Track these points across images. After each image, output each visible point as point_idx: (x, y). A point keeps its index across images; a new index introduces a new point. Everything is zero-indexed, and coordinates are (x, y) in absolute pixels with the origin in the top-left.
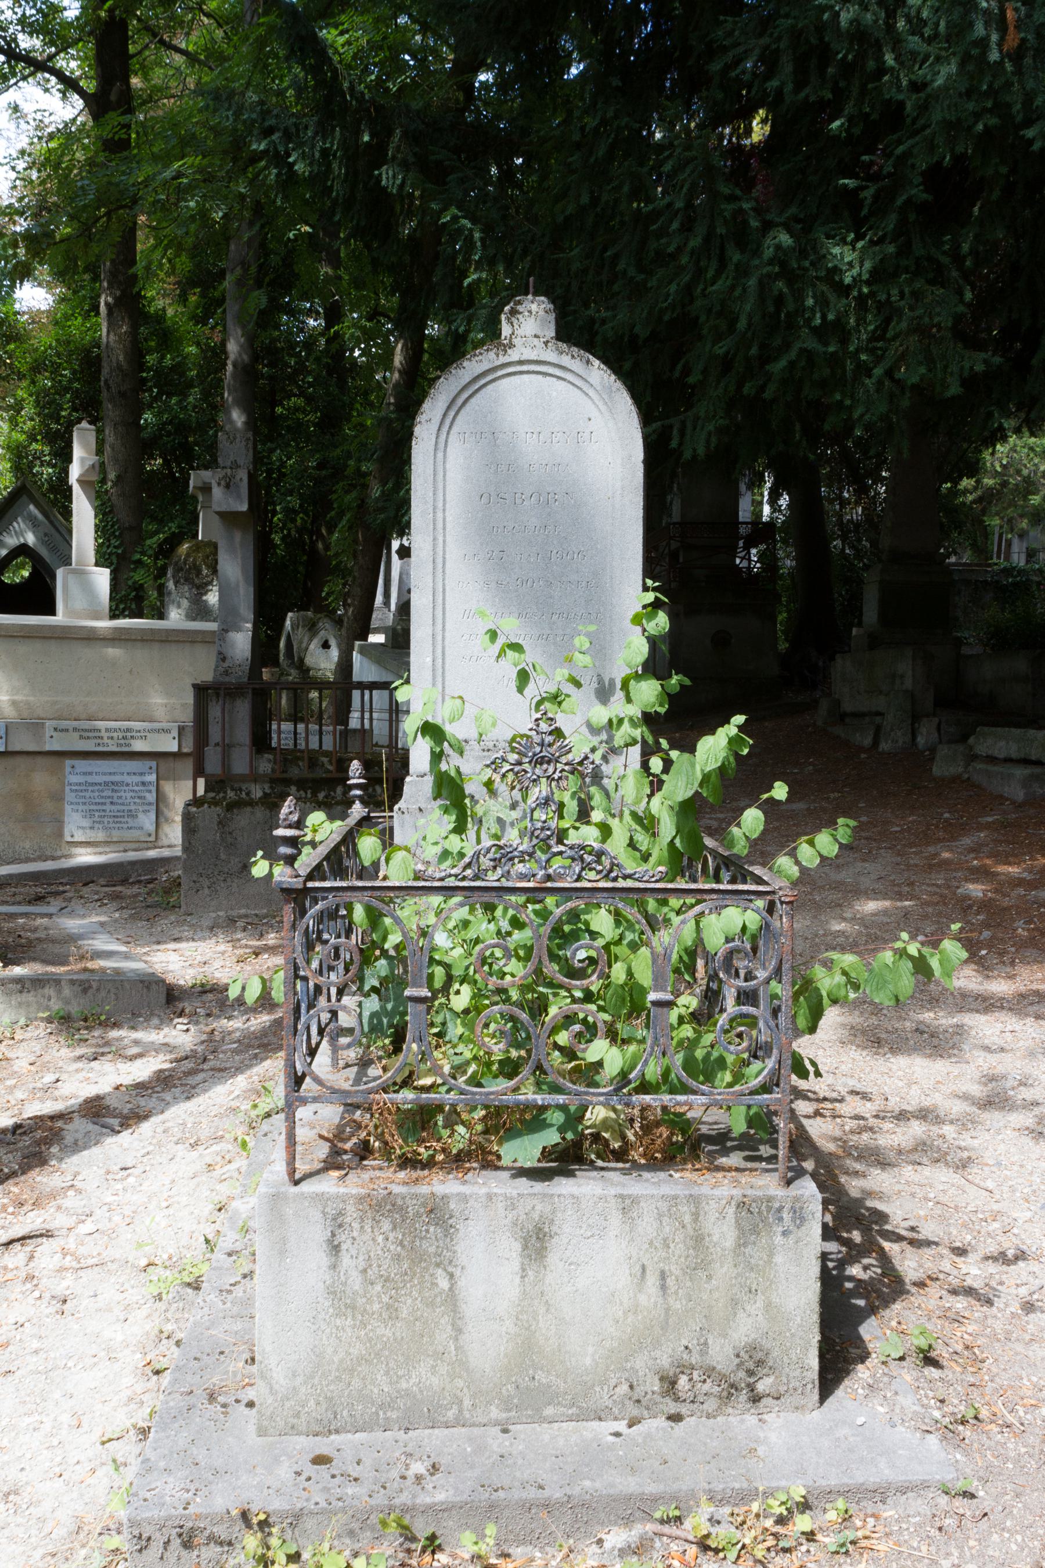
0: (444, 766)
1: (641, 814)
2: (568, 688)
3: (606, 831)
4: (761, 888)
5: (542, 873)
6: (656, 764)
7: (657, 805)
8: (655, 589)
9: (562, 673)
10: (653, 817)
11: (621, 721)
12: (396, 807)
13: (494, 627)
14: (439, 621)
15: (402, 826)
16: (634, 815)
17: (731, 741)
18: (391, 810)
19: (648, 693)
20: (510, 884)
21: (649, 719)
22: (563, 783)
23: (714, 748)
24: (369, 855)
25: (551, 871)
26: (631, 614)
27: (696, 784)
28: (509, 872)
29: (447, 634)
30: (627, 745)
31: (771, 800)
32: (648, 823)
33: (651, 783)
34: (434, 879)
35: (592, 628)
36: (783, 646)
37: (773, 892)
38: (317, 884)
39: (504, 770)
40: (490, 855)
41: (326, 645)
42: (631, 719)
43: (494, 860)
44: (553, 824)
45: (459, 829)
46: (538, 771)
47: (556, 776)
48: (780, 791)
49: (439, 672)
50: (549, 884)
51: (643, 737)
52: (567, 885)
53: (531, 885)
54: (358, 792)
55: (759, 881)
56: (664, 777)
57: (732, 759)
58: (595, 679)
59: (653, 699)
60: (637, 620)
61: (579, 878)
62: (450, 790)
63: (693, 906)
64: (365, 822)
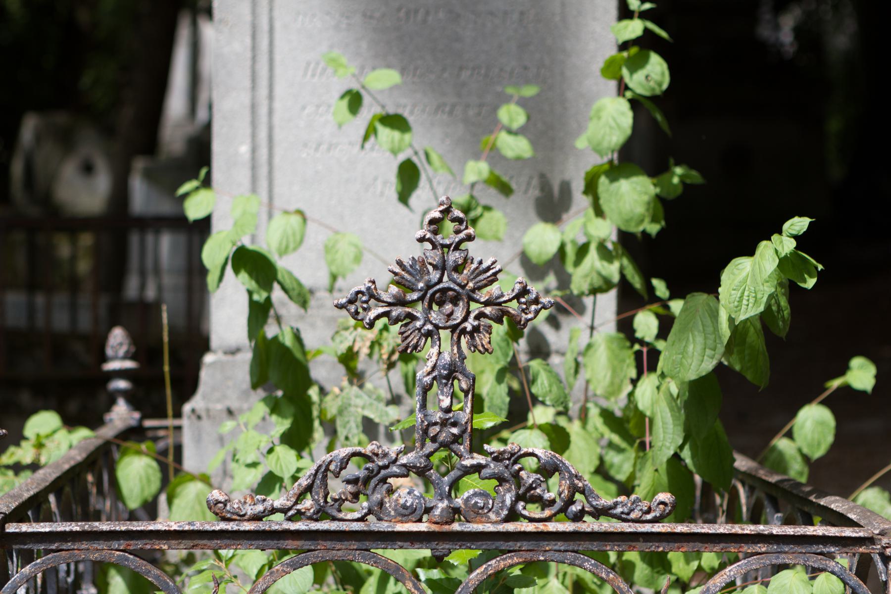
0: (270, 330)
1: (618, 413)
2: (490, 196)
3: (559, 438)
4: (848, 532)
5: (443, 505)
6: (646, 323)
7: (647, 392)
8: (643, 15)
9: (477, 170)
10: (641, 416)
11: (582, 251)
12: (187, 408)
13: (355, 86)
14: (263, 83)
15: (198, 440)
16: (607, 415)
17: (784, 263)
18: (178, 414)
19: (633, 198)
20: (384, 526)
21: (629, 243)
22: (482, 339)
23: (751, 281)
24: (136, 491)
25: (459, 502)
26: (600, 64)
27: (721, 349)
28: (381, 504)
29: (277, 105)
30: (594, 291)
31: (847, 389)
32: (630, 426)
33: (638, 355)
34: (242, 517)
35: (530, 91)
36: (836, 171)
37: (869, 541)
38: (25, 528)
39: (372, 314)
40: (346, 473)
41: (88, 169)
42: (602, 247)
43: (354, 481)
44: (464, 417)
45: (297, 439)
46: (434, 316)
47: (468, 326)
48: (861, 375)
49: (263, 171)
50: (456, 527)
51: (623, 276)
52: (489, 528)
53: (423, 527)
54: (122, 384)
55: (842, 520)
56: (660, 345)
57: (784, 302)
58: (535, 182)
59: (640, 209)
60: (611, 70)
61: (513, 516)
62: (281, 373)
63: (714, 572)
64: (134, 434)
